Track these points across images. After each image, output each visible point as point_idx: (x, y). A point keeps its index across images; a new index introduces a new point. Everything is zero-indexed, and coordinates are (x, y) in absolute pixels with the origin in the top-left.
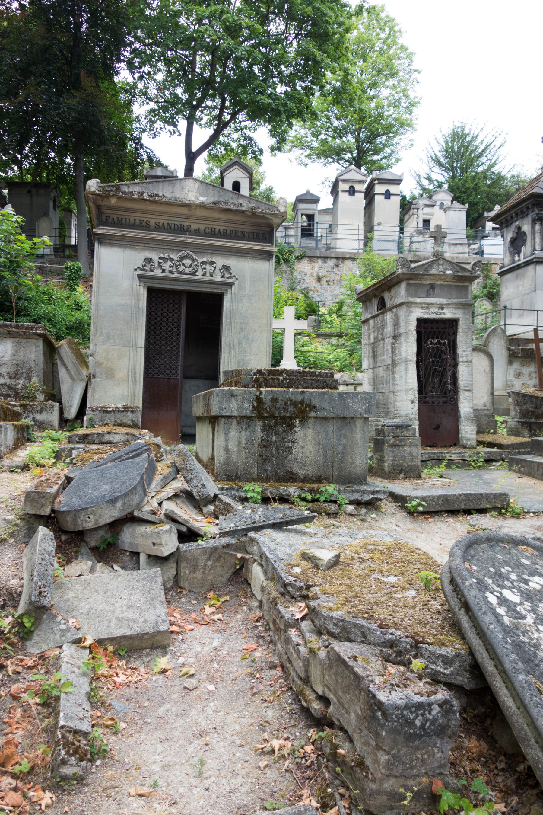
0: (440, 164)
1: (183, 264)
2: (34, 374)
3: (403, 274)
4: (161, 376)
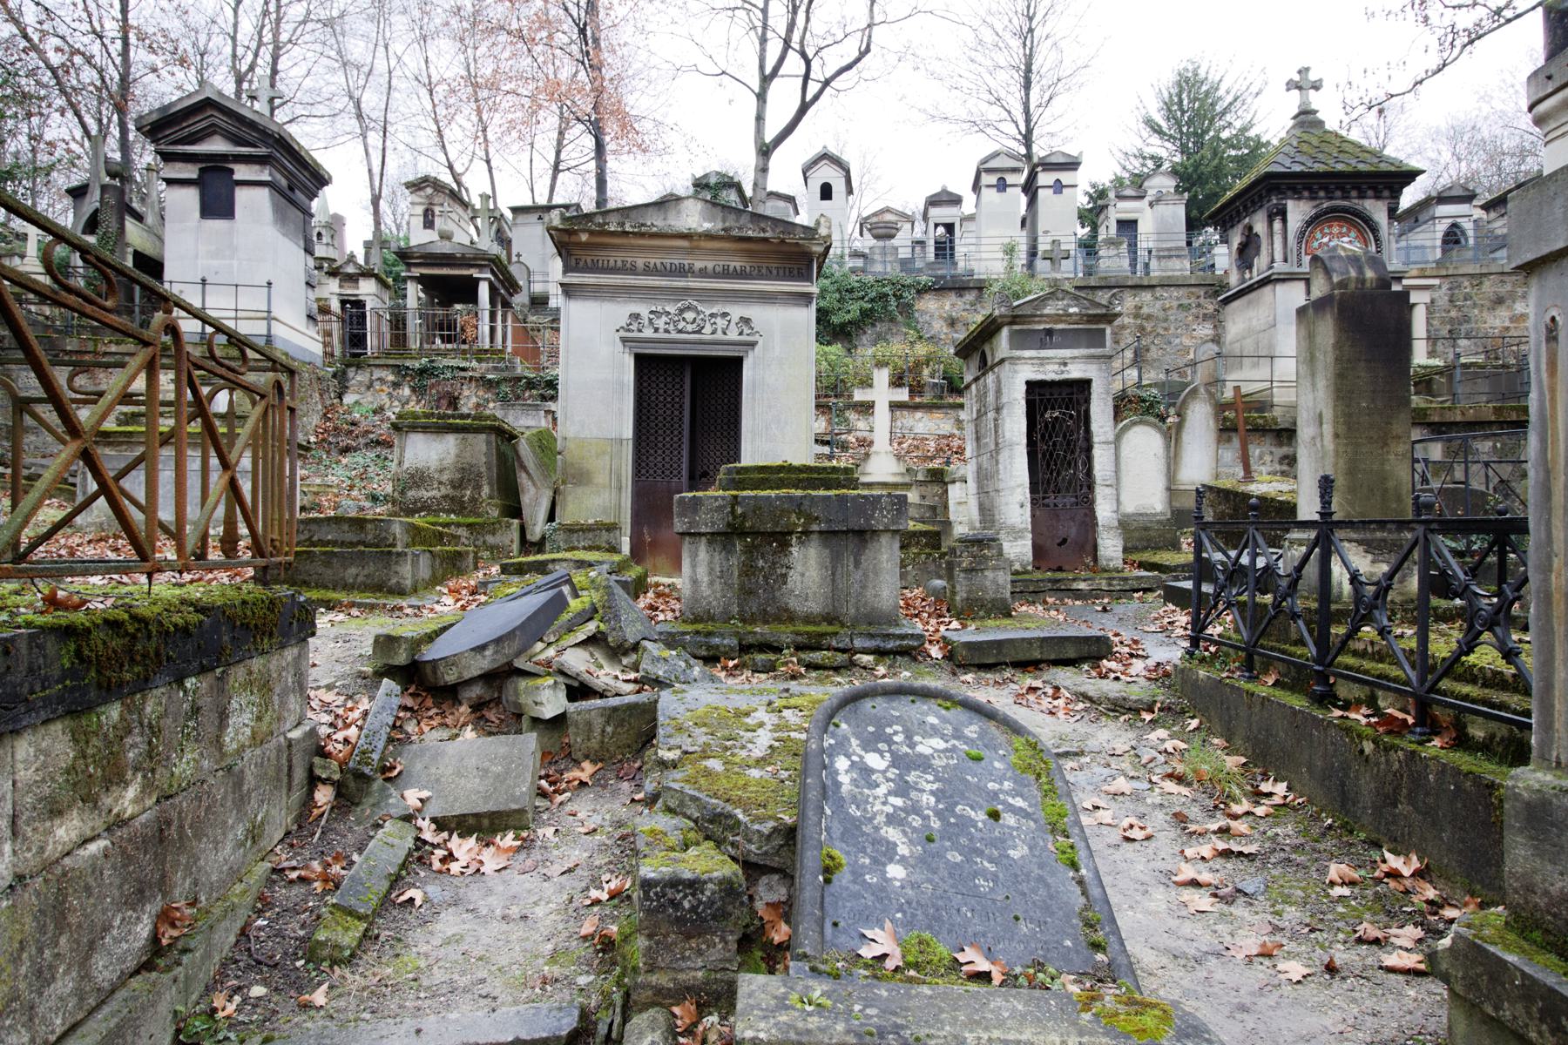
0: (1158, 131)
2: (484, 482)
3: (1001, 316)
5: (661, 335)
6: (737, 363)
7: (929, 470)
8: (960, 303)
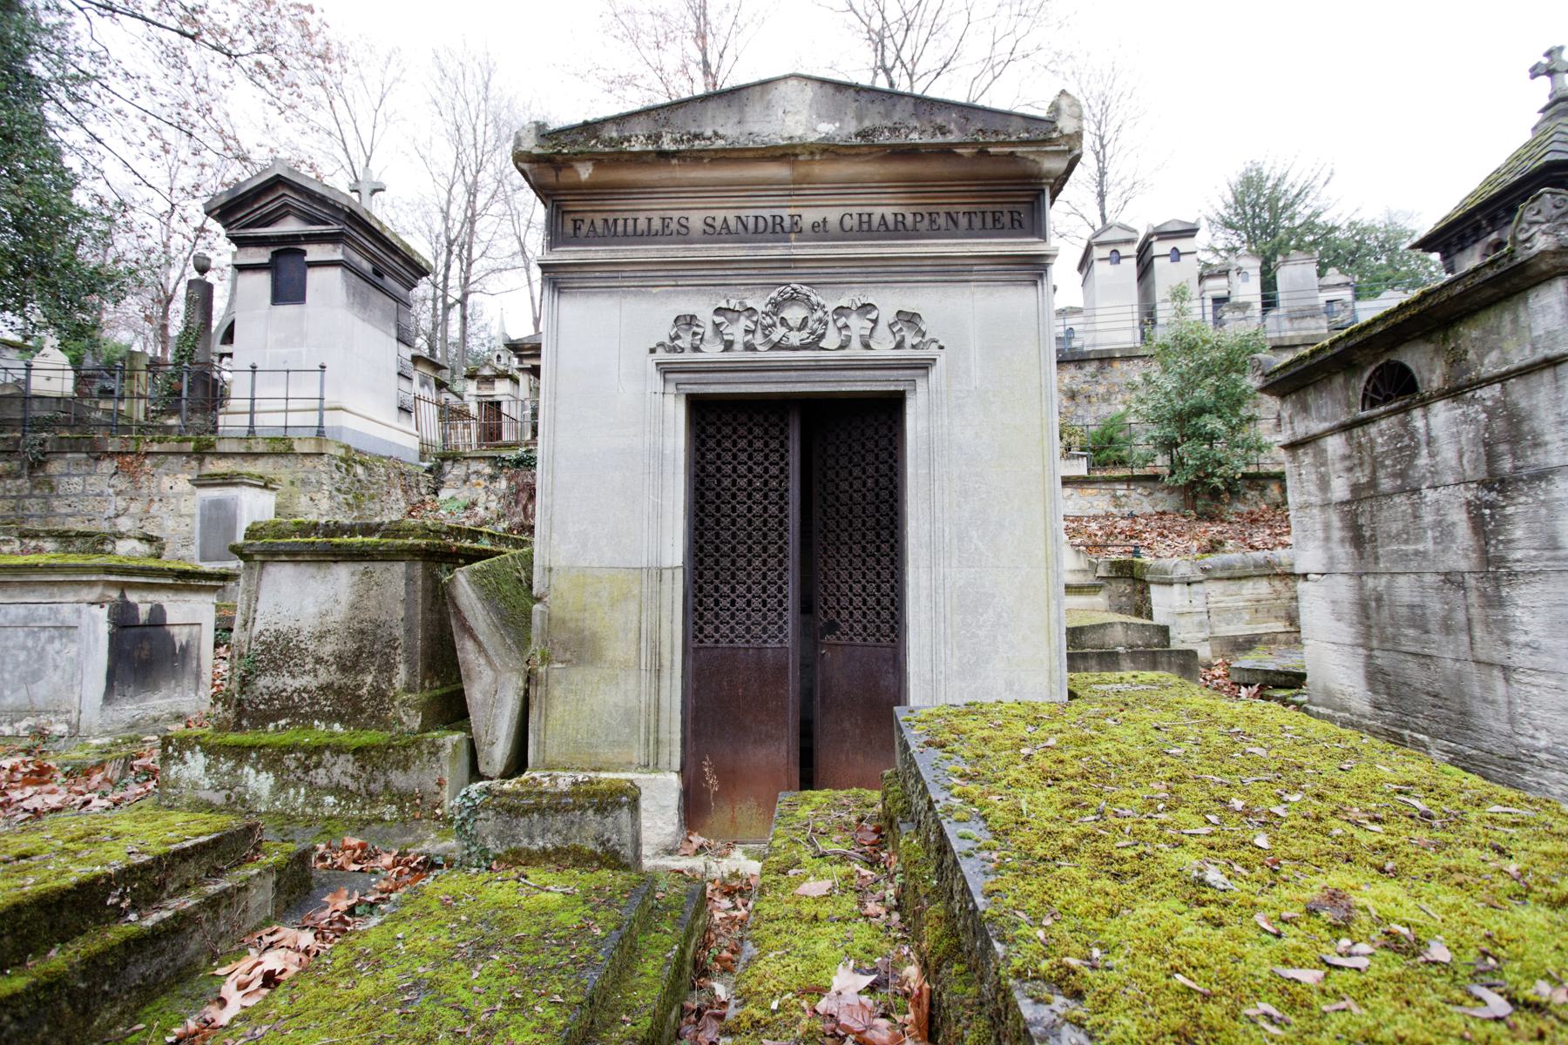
1: (783, 321)
4: (739, 643)
5: (738, 354)
6: (891, 406)
7: (1113, 564)
8: (1080, 374)
